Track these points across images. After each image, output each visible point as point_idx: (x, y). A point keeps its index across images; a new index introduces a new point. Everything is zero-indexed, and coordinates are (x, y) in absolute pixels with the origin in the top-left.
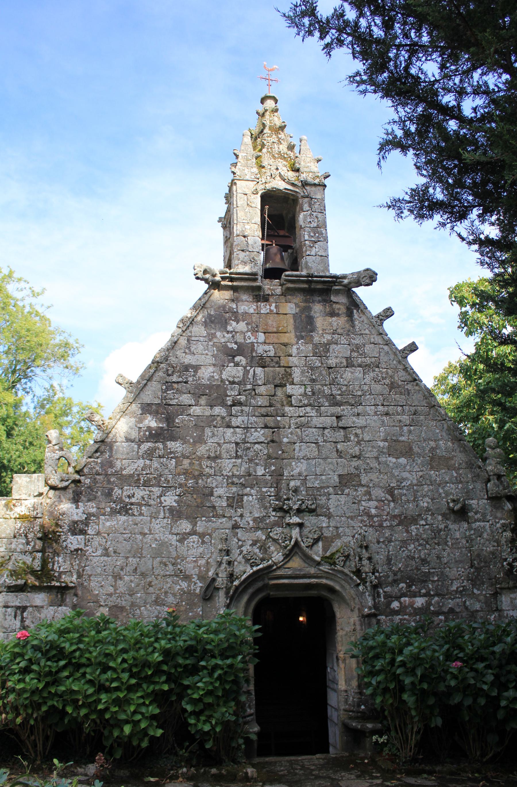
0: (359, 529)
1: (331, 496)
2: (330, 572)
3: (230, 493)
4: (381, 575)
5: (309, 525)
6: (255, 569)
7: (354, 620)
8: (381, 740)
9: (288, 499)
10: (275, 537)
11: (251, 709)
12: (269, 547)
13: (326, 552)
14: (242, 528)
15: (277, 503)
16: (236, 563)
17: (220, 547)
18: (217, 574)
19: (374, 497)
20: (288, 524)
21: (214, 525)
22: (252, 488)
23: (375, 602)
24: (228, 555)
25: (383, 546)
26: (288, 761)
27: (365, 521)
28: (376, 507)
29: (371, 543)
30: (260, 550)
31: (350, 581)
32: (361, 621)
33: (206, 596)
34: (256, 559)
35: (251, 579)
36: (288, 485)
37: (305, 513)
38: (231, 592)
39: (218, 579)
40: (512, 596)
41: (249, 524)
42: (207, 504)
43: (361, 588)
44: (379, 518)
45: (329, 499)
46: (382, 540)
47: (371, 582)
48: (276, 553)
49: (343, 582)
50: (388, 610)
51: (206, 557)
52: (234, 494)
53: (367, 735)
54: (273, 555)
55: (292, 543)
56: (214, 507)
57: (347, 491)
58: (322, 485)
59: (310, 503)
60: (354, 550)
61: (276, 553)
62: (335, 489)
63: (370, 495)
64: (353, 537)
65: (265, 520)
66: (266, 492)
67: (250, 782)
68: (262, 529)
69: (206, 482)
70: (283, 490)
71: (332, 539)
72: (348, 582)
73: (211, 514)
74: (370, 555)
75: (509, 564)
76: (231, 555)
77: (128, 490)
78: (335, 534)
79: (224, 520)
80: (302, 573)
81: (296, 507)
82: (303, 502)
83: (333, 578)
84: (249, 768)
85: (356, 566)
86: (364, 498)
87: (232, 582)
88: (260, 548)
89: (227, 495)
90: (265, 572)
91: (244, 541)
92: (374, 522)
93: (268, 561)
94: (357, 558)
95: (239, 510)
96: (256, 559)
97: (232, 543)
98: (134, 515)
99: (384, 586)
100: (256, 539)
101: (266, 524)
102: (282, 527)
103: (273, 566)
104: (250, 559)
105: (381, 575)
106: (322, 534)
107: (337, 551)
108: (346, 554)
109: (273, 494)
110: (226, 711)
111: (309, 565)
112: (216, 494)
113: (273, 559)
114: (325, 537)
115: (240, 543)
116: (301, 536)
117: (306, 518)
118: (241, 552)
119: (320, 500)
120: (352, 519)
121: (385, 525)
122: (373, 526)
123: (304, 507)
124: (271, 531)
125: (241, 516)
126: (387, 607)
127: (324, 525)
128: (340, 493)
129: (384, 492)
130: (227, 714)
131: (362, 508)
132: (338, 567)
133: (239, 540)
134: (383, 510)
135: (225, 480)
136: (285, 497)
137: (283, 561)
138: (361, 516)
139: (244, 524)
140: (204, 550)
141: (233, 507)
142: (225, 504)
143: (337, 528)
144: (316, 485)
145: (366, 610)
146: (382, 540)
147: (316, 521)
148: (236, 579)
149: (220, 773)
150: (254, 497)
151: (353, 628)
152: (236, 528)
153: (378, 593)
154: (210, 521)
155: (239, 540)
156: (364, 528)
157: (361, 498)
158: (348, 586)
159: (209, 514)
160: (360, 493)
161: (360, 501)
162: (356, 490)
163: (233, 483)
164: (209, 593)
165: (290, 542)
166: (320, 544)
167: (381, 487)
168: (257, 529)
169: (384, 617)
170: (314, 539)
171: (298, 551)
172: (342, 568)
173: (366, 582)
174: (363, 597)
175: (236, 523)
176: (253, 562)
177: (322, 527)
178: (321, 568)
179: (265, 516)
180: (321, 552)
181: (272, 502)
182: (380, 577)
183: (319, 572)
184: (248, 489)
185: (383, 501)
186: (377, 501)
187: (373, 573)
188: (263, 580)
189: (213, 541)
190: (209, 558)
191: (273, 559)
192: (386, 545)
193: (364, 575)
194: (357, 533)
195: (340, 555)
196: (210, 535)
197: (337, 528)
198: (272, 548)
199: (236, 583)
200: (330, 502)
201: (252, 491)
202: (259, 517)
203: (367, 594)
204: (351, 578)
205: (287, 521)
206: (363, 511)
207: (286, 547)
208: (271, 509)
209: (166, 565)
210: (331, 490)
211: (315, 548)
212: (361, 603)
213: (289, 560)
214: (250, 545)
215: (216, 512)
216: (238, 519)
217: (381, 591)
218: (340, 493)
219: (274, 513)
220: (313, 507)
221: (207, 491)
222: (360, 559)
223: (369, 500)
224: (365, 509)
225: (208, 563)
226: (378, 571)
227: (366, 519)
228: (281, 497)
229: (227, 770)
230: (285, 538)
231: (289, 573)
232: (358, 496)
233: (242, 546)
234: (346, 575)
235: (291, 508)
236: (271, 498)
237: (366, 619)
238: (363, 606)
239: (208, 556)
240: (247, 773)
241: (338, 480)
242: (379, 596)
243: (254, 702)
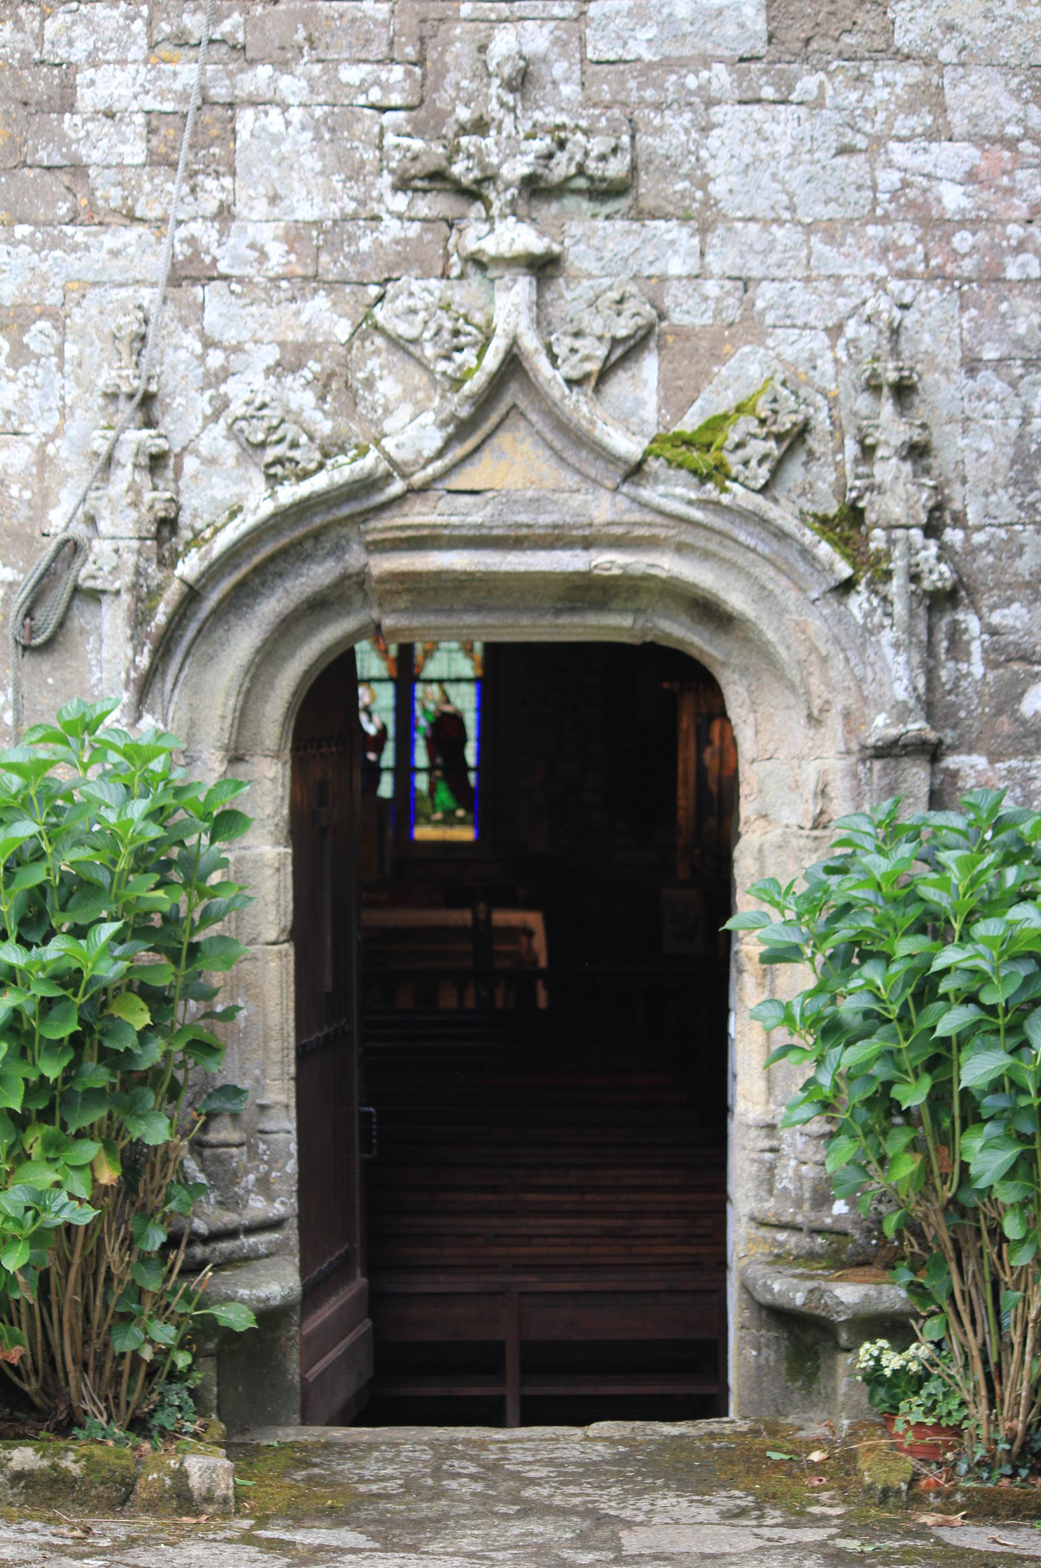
0: (867, 290)
1: (718, 113)
2: (698, 515)
3: (162, 95)
4: (978, 538)
5: (594, 267)
6: (289, 493)
7: (823, 773)
8: (892, 1361)
9: (480, 126)
10: (404, 329)
11: (271, 1198)
12: (369, 383)
13: (681, 411)
14: (225, 278)
15: (417, 144)
16: (190, 464)
17: (106, 378)
18: (91, 520)
19: (958, 121)
20: (478, 262)
21: (74, 264)
22: (283, 66)
23: (931, 675)
24: (149, 423)
25: (998, 387)
26: (432, 1445)
27: (902, 252)
28: (971, 177)
29: (933, 367)
30: (322, 398)
31: (801, 567)
32: (855, 775)
33: (33, 633)
34: (294, 445)
35: (268, 549)
36: (483, 49)
37: (570, 202)
38: (160, 618)
39: (96, 544)
41: (264, 256)
42: (43, 157)
43: (858, 603)
44: (983, 237)
45: (705, 130)
46: (990, 353)
47: (915, 578)
48: (405, 411)
49: (766, 573)
50: (1005, 725)
51: (38, 428)
52: (184, 97)
53: (844, 1337)
54: (388, 425)
55: (492, 361)
56: (78, 169)
57: (808, 84)
58: (673, 50)
59: (598, 145)
60: (833, 402)
61: (405, 411)
62: (743, 75)
63: (941, 108)
64: (835, 331)
65: (352, 239)
66: (363, 88)
67: (197, 1514)
68: (331, 286)
69: (39, 38)
70: (452, 77)
71: (718, 341)
72: (789, 573)
73: (63, 209)
74: (917, 435)
76: (167, 424)
78: (733, 313)
79: (131, 235)
80: (545, 519)
81: (516, 169)
82: (562, 144)
83: (713, 546)
84: (197, 1452)
85: (840, 489)
86: (903, 125)
87: (168, 562)
88: (322, 386)
89: (151, 103)
90: (346, 511)
91: (238, 349)
92: (956, 256)
93: (363, 452)
94: (851, 448)
95: (210, 183)
96: (294, 445)
97: (170, 357)
99: (986, 601)
100: (300, 336)
101: (355, 258)
102: (445, 275)
103: (388, 478)
104: (263, 445)
105: (978, 538)
106: (662, 316)
107: (739, 409)
108: (786, 422)
109: (396, 99)
110: (57, 1185)
111: (585, 477)
112: (87, 99)
113: (388, 444)
114: (683, 334)
115: (216, 359)
116: (542, 322)
117: (575, 228)
118: (221, 406)
119: (660, 131)
120: (830, 238)
121: (1012, 273)
122: (948, 279)
123: (562, 167)
124: (381, 298)
125: (225, 214)
126: (999, 711)
127: (676, 266)
128: (768, 92)
129: (1016, 93)
130: (64, 1198)
131: (889, 179)
132: (738, 495)
133: (209, 343)
134: (1010, 191)
135: (138, 26)
136: (464, 114)
137: (440, 454)
138: (885, 219)
139: (237, 260)
140: (23, 395)
141: (173, 165)
142: (135, 152)
143: (747, 283)
144: (639, 48)
145: (881, 720)
146: (990, 353)
147: (630, 244)
148: (188, 545)
149: (54, 1467)
150: (296, 114)
151: (814, 810)
152: (195, 280)
153: (956, 634)
154: (56, 243)
155: (209, 343)
156: (894, 285)
157: (889, 122)
158: (793, 594)
159: (52, 205)
160: (883, 94)
161: (878, 141)
162: (859, 78)
163: (182, 41)
164: (48, 617)
165: (480, 356)
166: (650, 365)
167: (1006, 67)
168: (314, 281)
169: (980, 761)
170: (615, 342)
171: (523, 404)
172: (759, 499)
173: (888, 575)
174: (870, 652)
175: (196, 253)
176: (279, 461)
177: (663, 279)
178: (646, 493)
179: (354, 217)
180: (650, 412)
181: (390, 139)
182: (972, 551)
183: (636, 516)
184: (264, 71)
185: (1011, 144)
186: (981, 140)
187: (932, 530)
188: (339, 550)
189: (71, 350)
190: (50, 438)
191: (388, 444)
192: (1013, 384)
193: (878, 539)
194: (854, 312)
195: (753, 426)
196: (57, 317)
197: (747, 283)
198: (387, 388)
199: (190, 567)
200: (713, 141)
201: (285, 82)
202: (317, 224)
203: (887, 637)
204: (806, 553)
205: (471, 245)
206: (894, 195)
207: (457, 383)
208: (387, 179)
210: (720, 77)
211: (620, 385)
212: (860, 681)
213: (477, 449)
214: (269, 371)
215: (92, 192)
216: (206, 233)
217: (972, 623)
218: (768, 92)
219: (400, 202)
220: (616, 168)
221: (40, 85)
222: (867, 452)
223: (932, 135)
224: (906, 184)
225: (43, 461)
226: (959, 520)
227: (907, 239)
228: (442, 116)
229: (89, 1457)
230: (456, 333)
231: (476, 518)
232: (869, 114)
233: (225, 374)
234: (781, 535)
235: (490, 178)
236: (389, 118)
237: (878, 765)
238: (865, 700)
239: (47, 426)
240: (181, 1475)
241: (759, 25)
242: (957, 647)
243: (291, 1166)
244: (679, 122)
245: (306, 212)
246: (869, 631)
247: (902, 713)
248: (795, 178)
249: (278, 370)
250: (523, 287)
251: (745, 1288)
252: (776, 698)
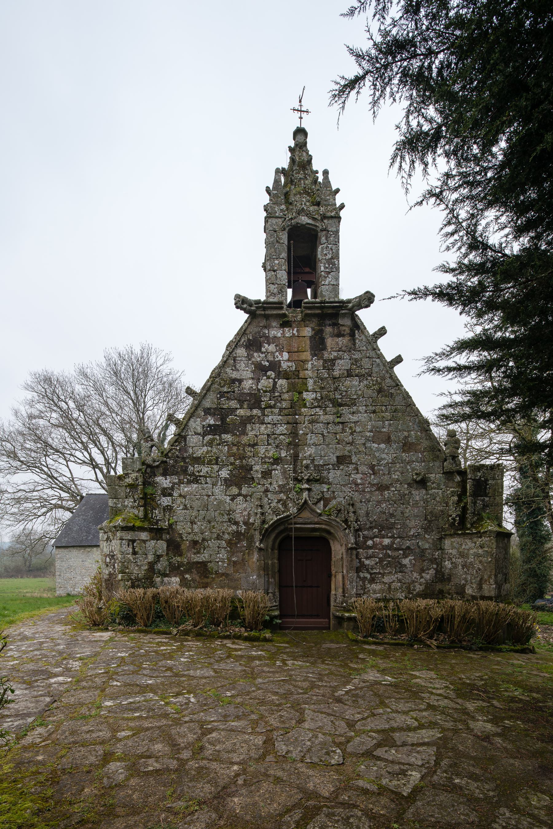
9: (301, 473)
28: (361, 479)
40: (452, 540)
43: (347, 531)
57: (341, 467)
63: (358, 470)
64: (344, 498)
68: (284, 493)
75: (453, 519)
77: (197, 467)
81: (306, 478)
88: (282, 504)
98: (201, 483)
114: (326, 498)
116: (309, 497)
118: (270, 507)
127: (325, 490)
131: (351, 479)
142: (260, 476)
144: (321, 463)
153: (359, 535)
161: (350, 474)
186: (362, 474)
187: (356, 522)
193: (350, 523)
204: (341, 525)
209: (223, 515)
210: (331, 466)
220: (318, 477)
223: (357, 473)
225: (249, 514)
233: (271, 503)
234: (338, 522)
235: (303, 479)
242: (359, 537)
244: (326, 472)
245: (280, 483)
246: (349, 534)
247: (352, 544)
248: (340, 479)
249: (277, 503)
250: (307, 492)
251: (333, 614)
252: (336, 543)
